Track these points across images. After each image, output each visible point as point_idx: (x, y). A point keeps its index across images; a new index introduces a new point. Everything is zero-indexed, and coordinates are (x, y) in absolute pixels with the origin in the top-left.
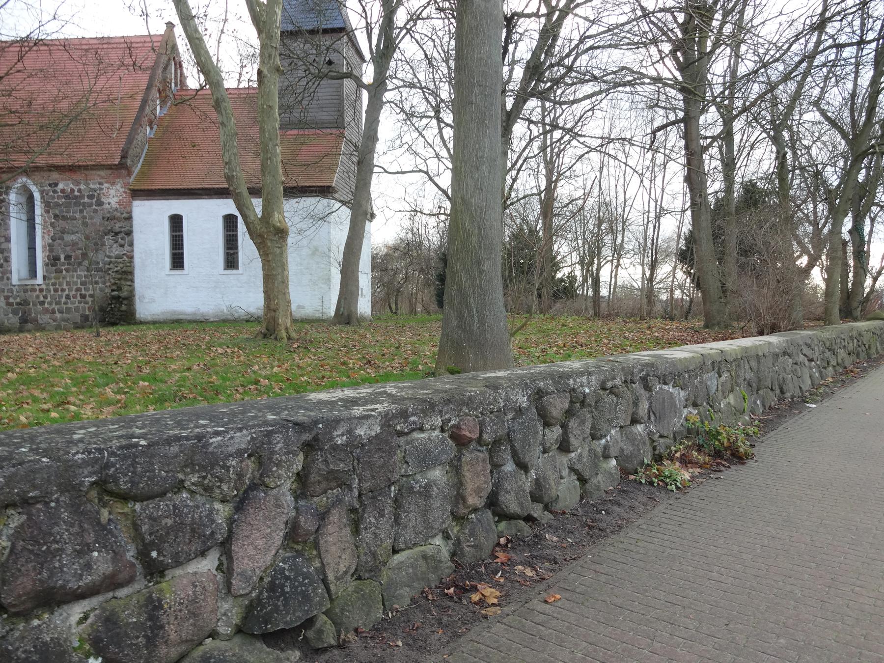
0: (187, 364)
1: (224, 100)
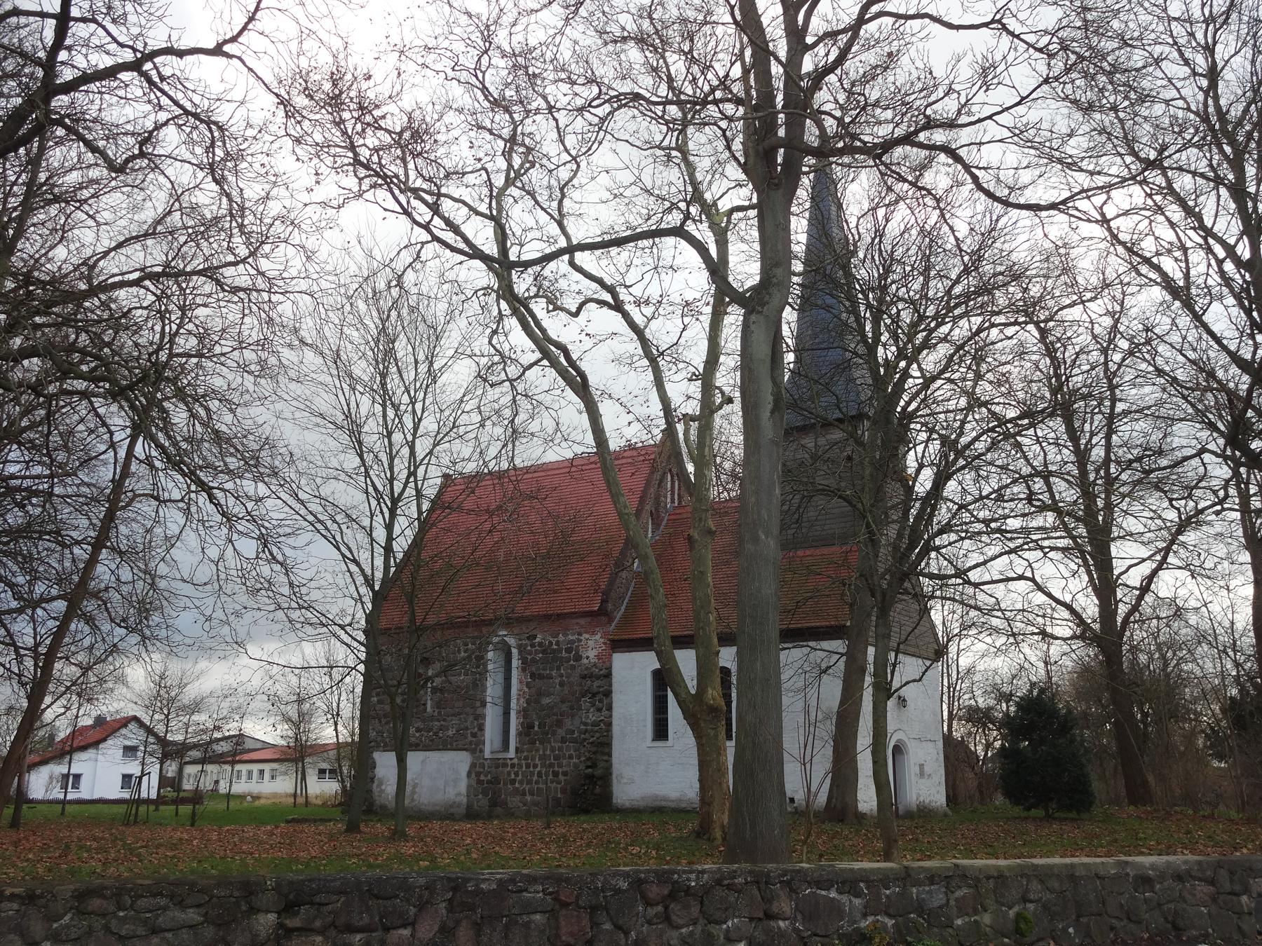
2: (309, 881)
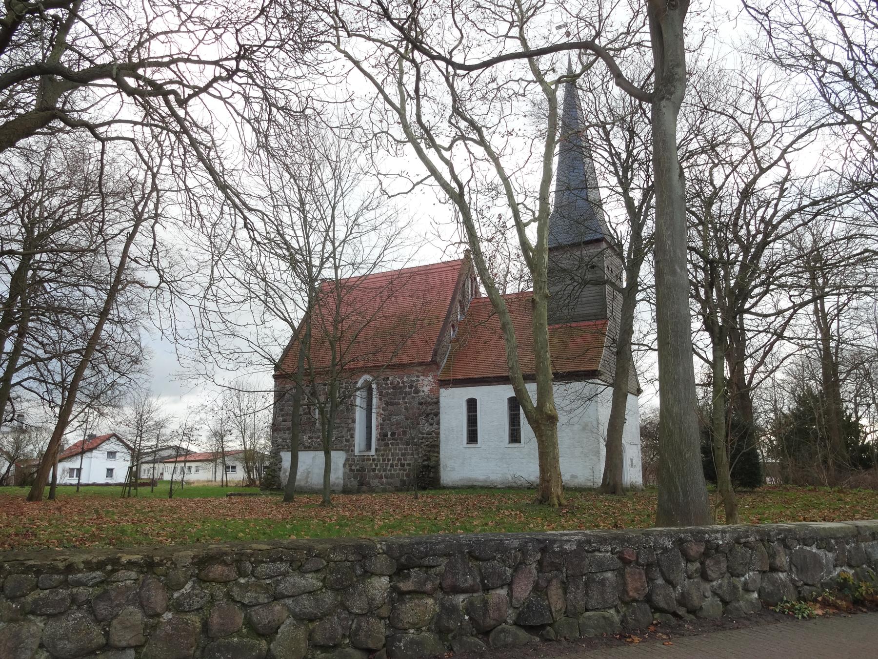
0: (484, 522)
1: (508, 324)
2: (418, 544)
